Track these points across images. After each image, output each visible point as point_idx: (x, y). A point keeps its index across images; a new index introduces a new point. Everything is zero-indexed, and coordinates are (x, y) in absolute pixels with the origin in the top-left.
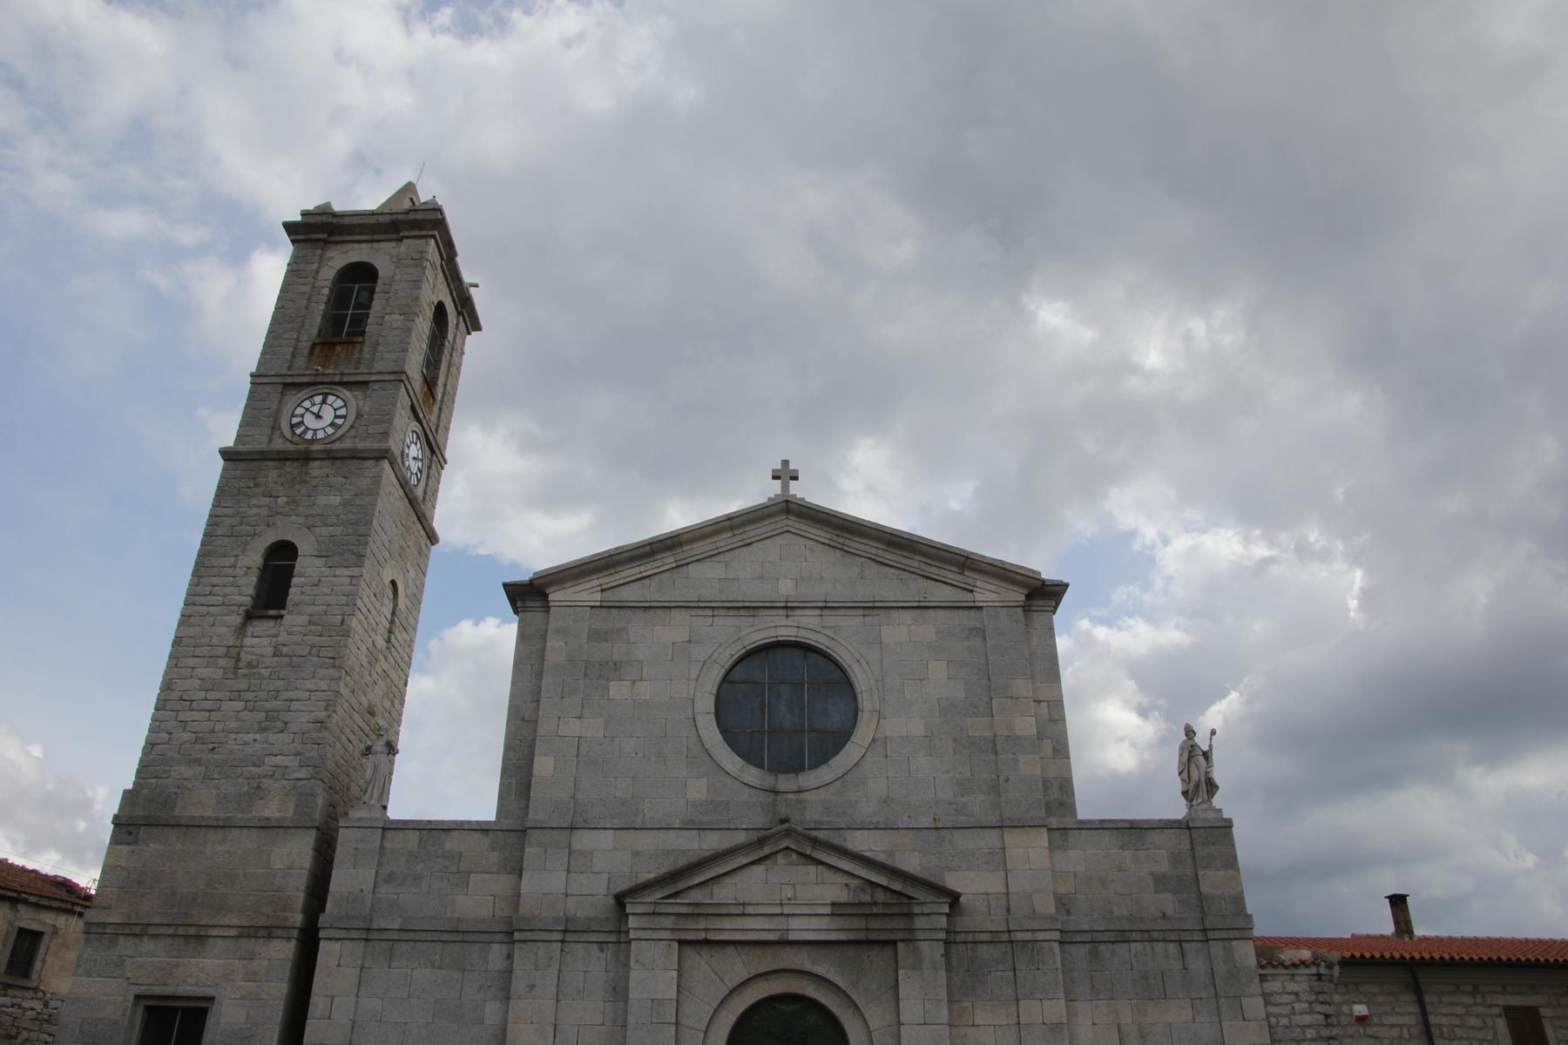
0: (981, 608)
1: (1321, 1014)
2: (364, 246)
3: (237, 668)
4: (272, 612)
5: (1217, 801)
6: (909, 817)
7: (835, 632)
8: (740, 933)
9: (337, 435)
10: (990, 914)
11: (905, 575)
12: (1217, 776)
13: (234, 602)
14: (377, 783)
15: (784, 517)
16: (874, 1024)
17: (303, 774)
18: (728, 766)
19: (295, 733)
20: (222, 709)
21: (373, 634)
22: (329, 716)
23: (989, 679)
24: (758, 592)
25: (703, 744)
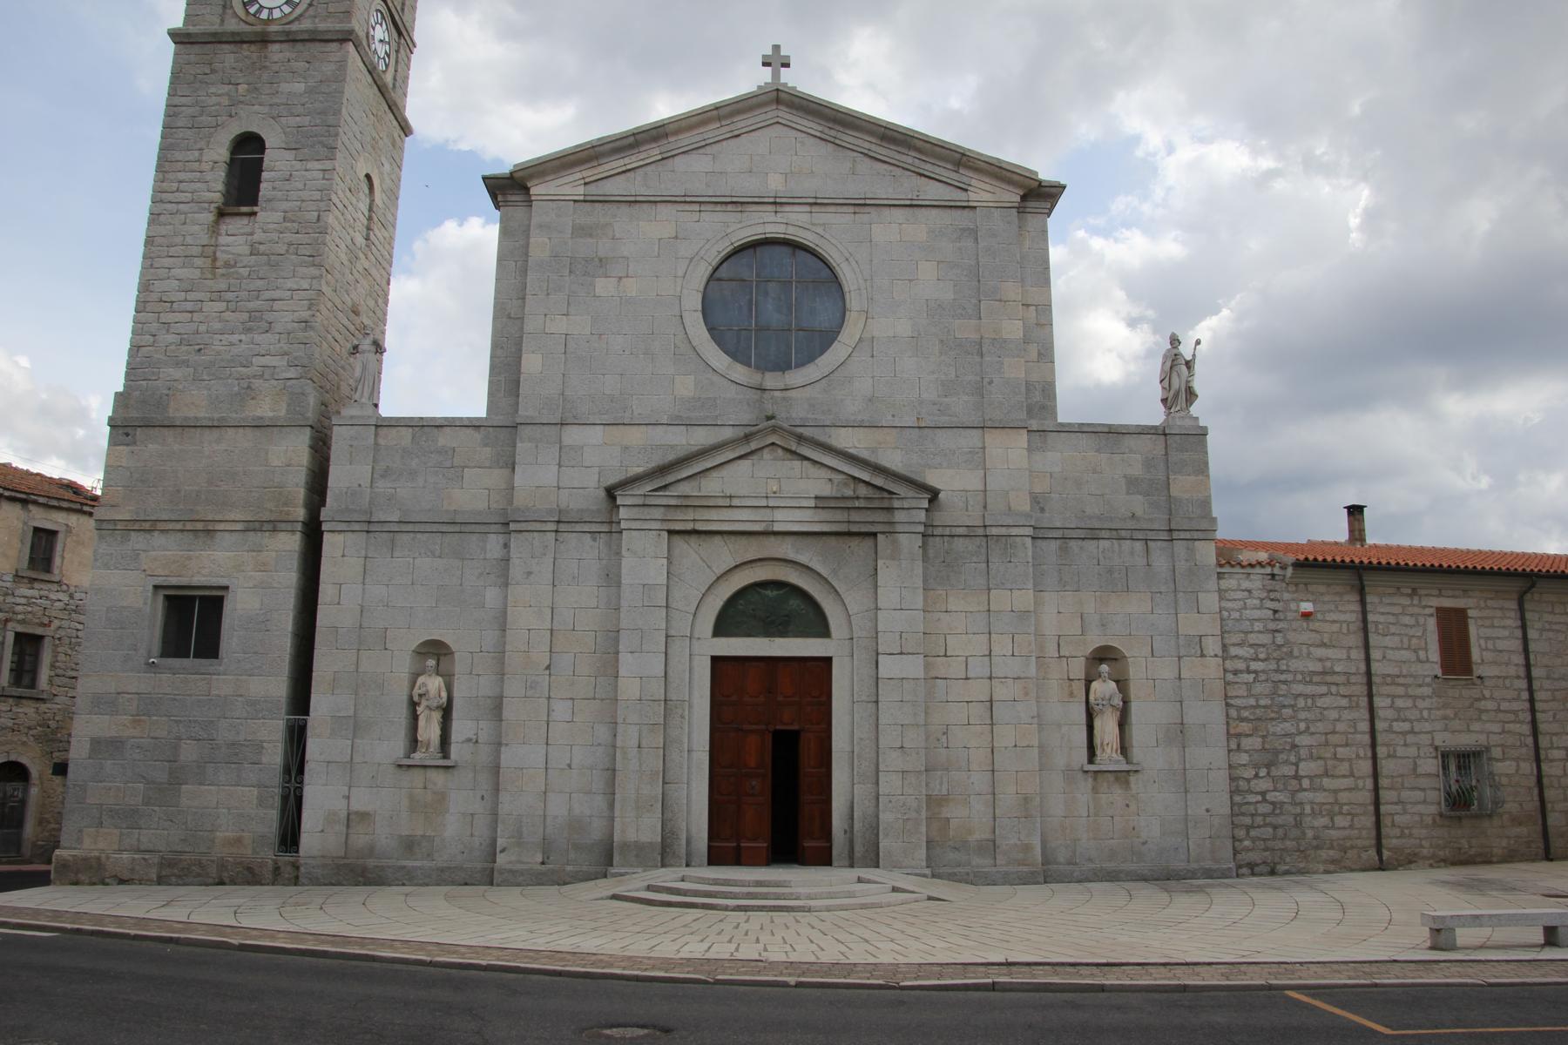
0: (975, 207)
4: (244, 209)
5: (1195, 410)
6: (893, 416)
8: (727, 523)
9: (294, 15)
10: (967, 510)
11: (898, 171)
12: (1197, 386)
13: (204, 199)
14: (366, 383)
15: (774, 107)
16: (853, 609)
17: (291, 373)
18: (715, 364)
20: (204, 310)
21: (351, 231)
22: (314, 316)
23: (979, 281)
24: (748, 187)
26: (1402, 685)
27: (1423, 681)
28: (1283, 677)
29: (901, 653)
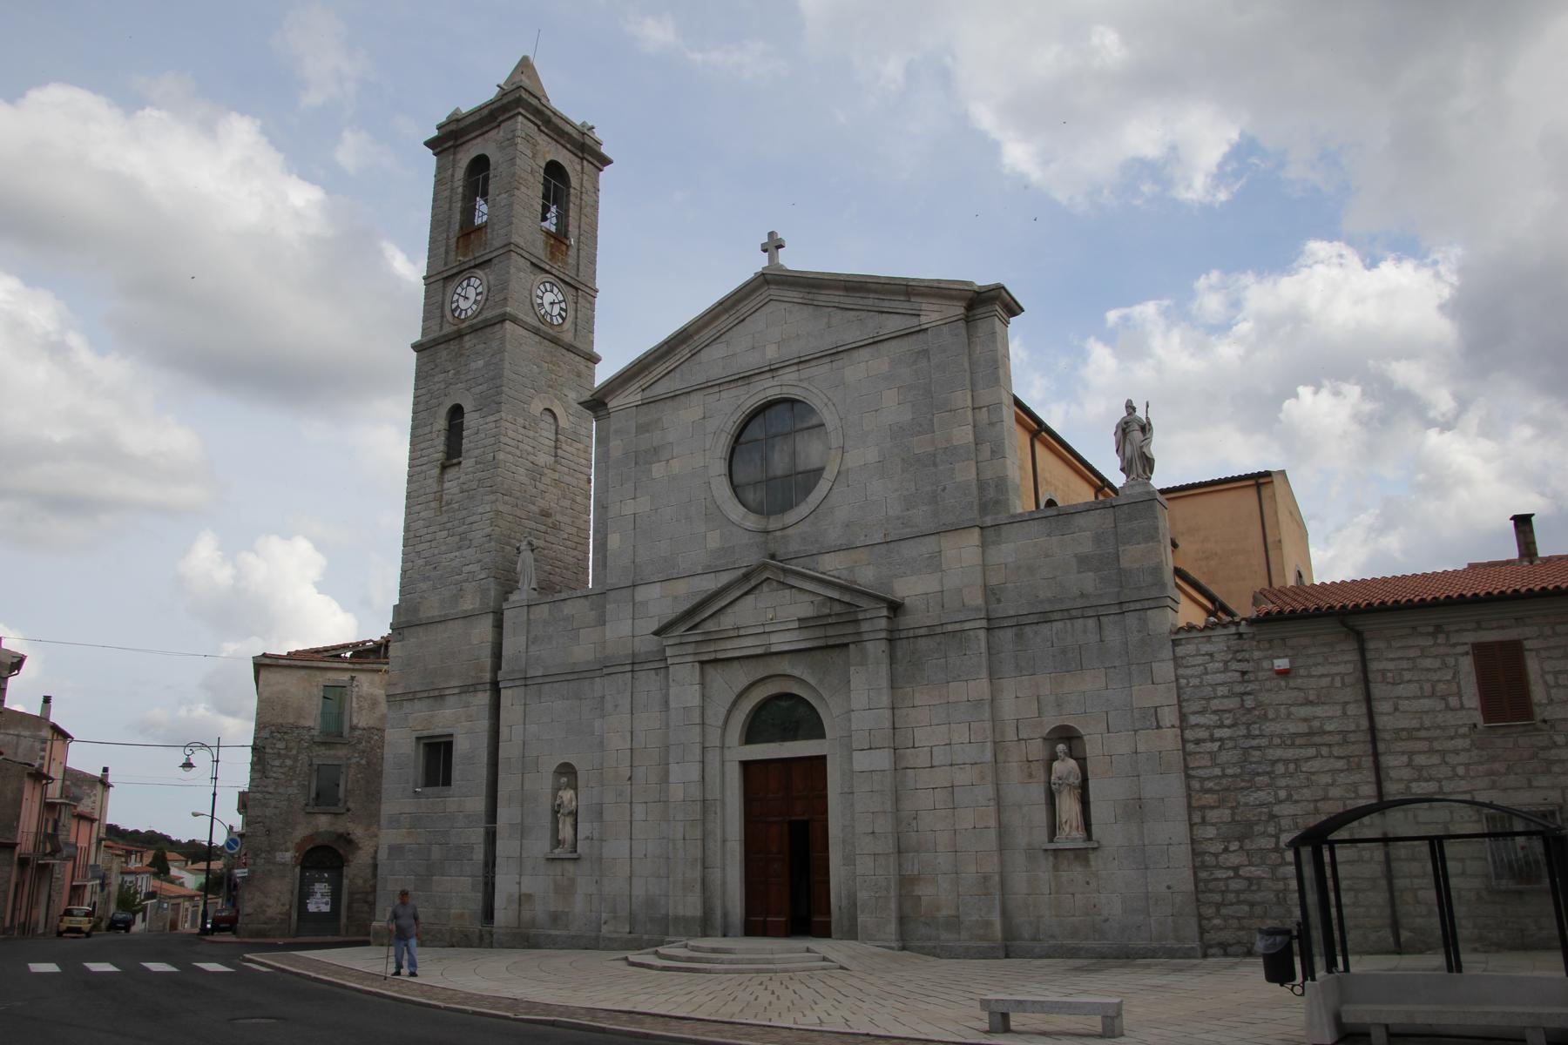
0: (927, 329)
1: (1236, 671)
2: (479, 140)
6: (866, 536)
9: (480, 307)
10: (928, 611)
11: (864, 314)
18: (733, 517)
24: (749, 361)
26: (1425, 739)
27: (1456, 732)
28: (1255, 743)
29: (871, 749)
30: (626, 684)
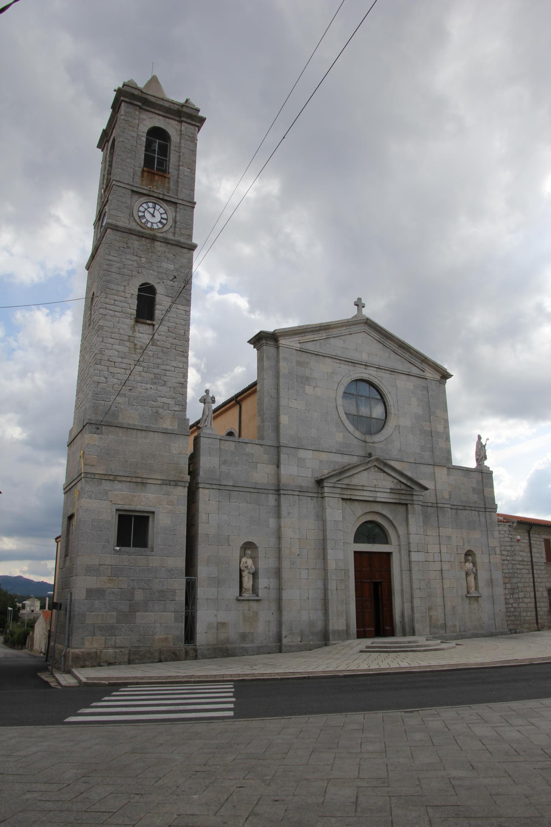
0: (427, 379)
3: (135, 349)
6: (407, 458)
7: (381, 379)
8: (361, 497)
10: (431, 496)
11: (403, 360)
13: (128, 312)
16: (401, 533)
19: (170, 388)
23: (429, 408)
24: (355, 356)
25: (340, 419)
29: (418, 551)
30: (295, 502)
